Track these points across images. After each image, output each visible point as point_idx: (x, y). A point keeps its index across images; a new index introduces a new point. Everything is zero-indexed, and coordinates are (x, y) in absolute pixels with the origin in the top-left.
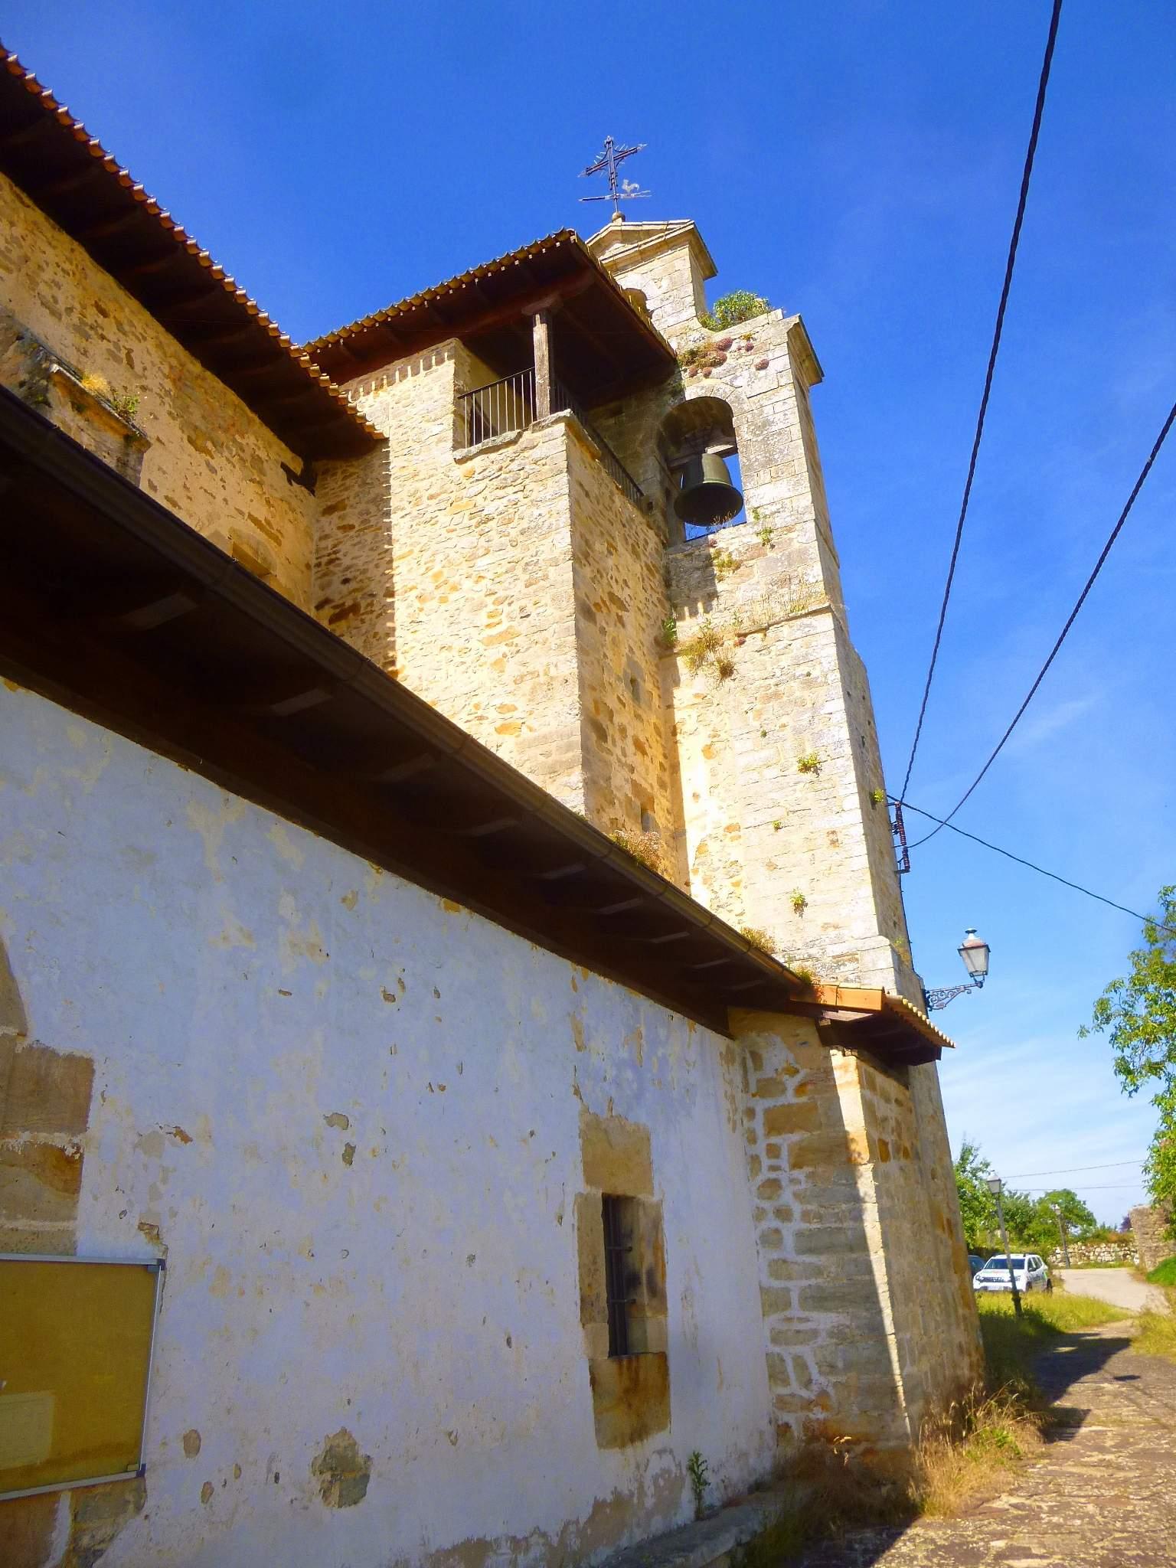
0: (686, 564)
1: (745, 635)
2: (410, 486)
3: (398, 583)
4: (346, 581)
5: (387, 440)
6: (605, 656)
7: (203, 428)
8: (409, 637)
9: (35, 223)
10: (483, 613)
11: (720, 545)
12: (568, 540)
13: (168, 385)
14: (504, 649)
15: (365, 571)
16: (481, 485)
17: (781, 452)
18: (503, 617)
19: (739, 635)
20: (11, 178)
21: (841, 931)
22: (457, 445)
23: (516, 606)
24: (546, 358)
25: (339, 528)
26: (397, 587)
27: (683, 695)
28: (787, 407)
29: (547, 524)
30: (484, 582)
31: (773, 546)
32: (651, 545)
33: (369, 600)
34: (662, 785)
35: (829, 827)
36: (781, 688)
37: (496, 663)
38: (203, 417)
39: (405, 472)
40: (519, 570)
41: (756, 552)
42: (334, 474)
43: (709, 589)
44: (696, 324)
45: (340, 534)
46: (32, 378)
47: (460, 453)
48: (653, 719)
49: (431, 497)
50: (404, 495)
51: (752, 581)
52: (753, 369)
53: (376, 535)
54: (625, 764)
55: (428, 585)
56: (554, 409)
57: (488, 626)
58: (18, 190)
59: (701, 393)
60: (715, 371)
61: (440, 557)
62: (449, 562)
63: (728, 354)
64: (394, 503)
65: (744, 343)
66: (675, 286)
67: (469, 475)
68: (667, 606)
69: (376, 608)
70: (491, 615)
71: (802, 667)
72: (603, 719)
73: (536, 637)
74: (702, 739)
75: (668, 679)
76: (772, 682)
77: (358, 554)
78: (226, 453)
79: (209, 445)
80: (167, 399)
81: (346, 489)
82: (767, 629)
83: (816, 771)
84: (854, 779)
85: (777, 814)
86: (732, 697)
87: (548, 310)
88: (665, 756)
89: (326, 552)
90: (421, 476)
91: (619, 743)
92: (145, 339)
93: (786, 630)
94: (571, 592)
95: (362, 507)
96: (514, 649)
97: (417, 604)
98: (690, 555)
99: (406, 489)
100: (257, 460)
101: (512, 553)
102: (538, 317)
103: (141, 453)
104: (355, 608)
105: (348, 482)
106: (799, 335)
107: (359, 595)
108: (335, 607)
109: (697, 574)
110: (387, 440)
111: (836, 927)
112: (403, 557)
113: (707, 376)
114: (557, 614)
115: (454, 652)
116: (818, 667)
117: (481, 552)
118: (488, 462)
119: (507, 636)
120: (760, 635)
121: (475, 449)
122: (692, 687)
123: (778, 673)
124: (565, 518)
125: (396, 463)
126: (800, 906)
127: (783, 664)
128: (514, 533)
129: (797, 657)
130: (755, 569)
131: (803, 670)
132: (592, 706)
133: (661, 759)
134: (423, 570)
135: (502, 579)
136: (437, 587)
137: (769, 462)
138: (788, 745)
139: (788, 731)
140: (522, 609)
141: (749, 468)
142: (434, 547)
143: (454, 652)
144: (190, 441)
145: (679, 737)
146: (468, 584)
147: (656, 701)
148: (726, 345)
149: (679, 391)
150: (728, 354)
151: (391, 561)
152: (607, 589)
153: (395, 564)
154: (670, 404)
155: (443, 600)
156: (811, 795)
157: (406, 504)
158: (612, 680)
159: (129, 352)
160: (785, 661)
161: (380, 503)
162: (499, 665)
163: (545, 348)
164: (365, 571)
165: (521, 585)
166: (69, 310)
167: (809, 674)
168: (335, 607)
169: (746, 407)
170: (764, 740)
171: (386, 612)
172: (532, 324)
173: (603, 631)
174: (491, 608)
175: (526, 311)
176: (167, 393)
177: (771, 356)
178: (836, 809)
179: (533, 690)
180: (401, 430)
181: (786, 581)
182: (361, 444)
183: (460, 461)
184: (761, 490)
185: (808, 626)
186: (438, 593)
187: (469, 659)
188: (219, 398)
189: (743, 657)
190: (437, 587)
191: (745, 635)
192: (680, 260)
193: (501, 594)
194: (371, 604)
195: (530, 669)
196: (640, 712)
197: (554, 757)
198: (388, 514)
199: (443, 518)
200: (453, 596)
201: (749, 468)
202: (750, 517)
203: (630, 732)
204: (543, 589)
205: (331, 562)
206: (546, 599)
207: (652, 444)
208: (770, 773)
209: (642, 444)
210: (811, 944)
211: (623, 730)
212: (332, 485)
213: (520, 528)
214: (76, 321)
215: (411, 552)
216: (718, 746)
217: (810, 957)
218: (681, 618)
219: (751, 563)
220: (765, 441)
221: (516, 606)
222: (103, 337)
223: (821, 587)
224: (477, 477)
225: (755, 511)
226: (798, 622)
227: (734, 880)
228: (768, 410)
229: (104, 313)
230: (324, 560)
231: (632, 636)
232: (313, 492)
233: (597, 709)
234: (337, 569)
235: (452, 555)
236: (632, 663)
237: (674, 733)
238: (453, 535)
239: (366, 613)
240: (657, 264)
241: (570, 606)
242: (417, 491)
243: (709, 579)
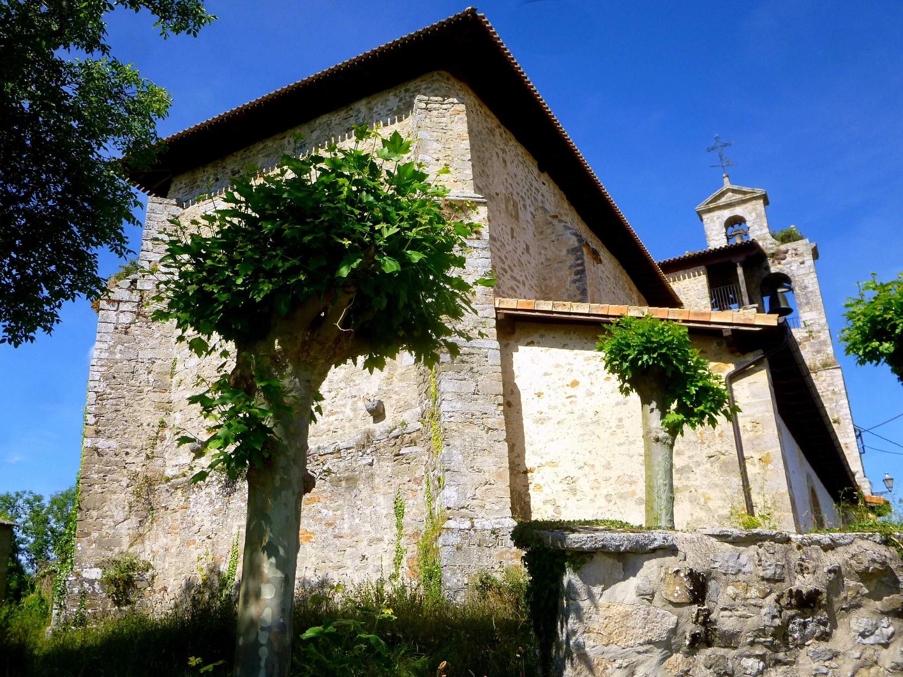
44: (769, 236)
56: (751, 302)
59: (777, 271)
60: (783, 262)
66: (758, 216)
131: (831, 388)
137: (808, 303)
141: (800, 305)
148: (786, 252)
149: (768, 268)
154: (765, 273)
172: (736, 267)
181: (818, 352)
184: (806, 314)
201: (800, 305)
228: (806, 282)
240: (749, 205)
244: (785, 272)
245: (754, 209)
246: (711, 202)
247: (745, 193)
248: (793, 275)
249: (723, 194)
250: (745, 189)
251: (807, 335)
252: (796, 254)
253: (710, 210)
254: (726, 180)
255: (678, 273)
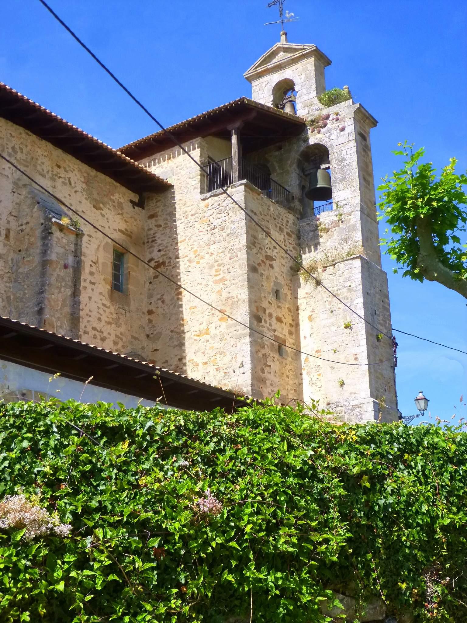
0: (307, 228)
1: (326, 267)
2: (184, 209)
3: (181, 253)
4: (159, 251)
5: (173, 186)
6: (262, 285)
7: (98, 199)
8: (185, 278)
9: (33, 141)
10: (214, 269)
11: (321, 220)
12: (245, 240)
13: (84, 186)
14: (222, 286)
15: (167, 247)
16: (211, 212)
17: (348, 174)
18: (221, 272)
19: (324, 267)
20: (24, 127)
21: (357, 395)
22: (202, 193)
23: (226, 268)
24: (237, 153)
25: (155, 226)
26: (180, 255)
27: (302, 292)
28: (352, 151)
29: (237, 232)
30: (214, 256)
31: (342, 222)
32: (291, 222)
33: (169, 260)
34: (291, 333)
35: (354, 353)
36: (339, 292)
37: (218, 292)
38: (98, 194)
39: (181, 202)
40: (227, 252)
41: (336, 224)
42: (152, 200)
43: (316, 241)
44: (316, 101)
45: (156, 229)
46: (45, 222)
47: (204, 196)
48: (287, 305)
49: (192, 215)
50: (181, 213)
51: (334, 238)
52: (339, 131)
53: (171, 231)
54: (271, 330)
55: (192, 256)
56: (241, 178)
57: (215, 275)
58: (27, 131)
59: (316, 141)
60: (322, 130)
61: (196, 243)
62: (200, 246)
63: (328, 121)
64: (178, 216)
65: (335, 117)
66: (307, 78)
67: (207, 206)
68: (298, 249)
69: (172, 264)
70: (217, 271)
71: (348, 282)
72: (260, 314)
73: (233, 282)
74: (307, 313)
75: (295, 286)
76: (336, 288)
77: (164, 239)
78: (108, 206)
79: (101, 205)
80: (84, 193)
81: (158, 207)
82: (335, 265)
83: (351, 329)
84: (365, 333)
85: (336, 346)
86: (320, 295)
87: (238, 128)
88: (293, 320)
89: (151, 236)
90: (187, 205)
91: (268, 321)
92: (74, 170)
93: (342, 266)
94: (246, 263)
95: (164, 216)
96: (225, 286)
97: (188, 264)
98: (308, 224)
99: (182, 210)
100: (120, 204)
101: (224, 244)
102: (233, 131)
103: (81, 238)
104: (163, 263)
105: (158, 204)
106: (361, 111)
107: (165, 257)
108: (155, 262)
109: (311, 234)
110: (173, 186)
111: (355, 394)
112: (181, 242)
113: (319, 132)
114: (241, 272)
115: (203, 286)
116: (354, 283)
117: (212, 242)
118: (214, 201)
119: (223, 280)
120: (332, 267)
121: (210, 194)
122: (305, 288)
123: (338, 285)
124: (244, 230)
125: (178, 197)
126: (342, 384)
127: (340, 281)
128: (225, 235)
129: (346, 278)
130: (335, 233)
132: (255, 310)
133: (291, 322)
134: (189, 249)
135: (220, 255)
136: (196, 257)
137: (343, 179)
138: (341, 316)
139: (341, 310)
140: (228, 269)
142: (194, 238)
143: (203, 286)
144: (94, 207)
145: (299, 311)
146: (207, 256)
147: (289, 297)
148: (327, 117)
149: (306, 140)
150: (328, 121)
151: (177, 243)
152: (264, 254)
153: (179, 244)
154: (303, 147)
155: (198, 263)
156: (348, 339)
157: (182, 218)
158: (266, 295)
159: (69, 178)
160: (341, 280)
161: (172, 215)
162: (219, 292)
163: (236, 147)
164: (167, 247)
165: (227, 258)
166: (48, 172)
167: (350, 286)
168: (155, 262)
169: (335, 150)
170: (332, 314)
171: (176, 266)
173: (262, 275)
174: (216, 267)
175: (229, 127)
176: (84, 190)
177: (346, 125)
178: (357, 345)
179: (232, 304)
180: (179, 182)
182: (162, 188)
183: (204, 200)
185: (351, 264)
186: (196, 259)
187: (208, 289)
188: (104, 180)
189: (325, 277)
190: (196, 257)
191: (326, 267)
192: (310, 64)
193: (220, 262)
194: (170, 262)
195: (231, 295)
196: (280, 304)
197: (240, 332)
198: (175, 221)
199: (197, 225)
200: (202, 261)
202: (334, 206)
203: (274, 315)
204: (236, 261)
205: (153, 241)
206: (237, 266)
207: (295, 166)
208: (334, 328)
209: (290, 166)
210: (346, 400)
211: (270, 315)
212: (152, 205)
213: (227, 233)
214: (51, 175)
215: (185, 239)
216: (314, 316)
217: (344, 406)
218: (305, 253)
219: (333, 229)
220: (342, 168)
221: (226, 268)
222: (60, 177)
223: (360, 243)
224: (210, 207)
225: (337, 203)
226: (347, 262)
227: (318, 373)
228: (344, 152)
229: (59, 167)
230: (150, 240)
231: (280, 268)
232: (143, 208)
233: (257, 310)
234: (155, 245)
235: (201, 243)
236: (276, 283)
237: (297, 310)
238: (201, 233)
239: (168, 266)
240: (299, 66)
241: (245, 269)
242: (186, 212)
243: (317, 237)
244: (323, 143)
245: (305, 70)
246: (259, 65)
247: (296, 50)
248: (332, 146)
249: (274, 54)
250: (295, 46)
251: (336, 219)
252: (337, 119)
253: (259, 75)
254: (283, 38)
255: (173, 149)
